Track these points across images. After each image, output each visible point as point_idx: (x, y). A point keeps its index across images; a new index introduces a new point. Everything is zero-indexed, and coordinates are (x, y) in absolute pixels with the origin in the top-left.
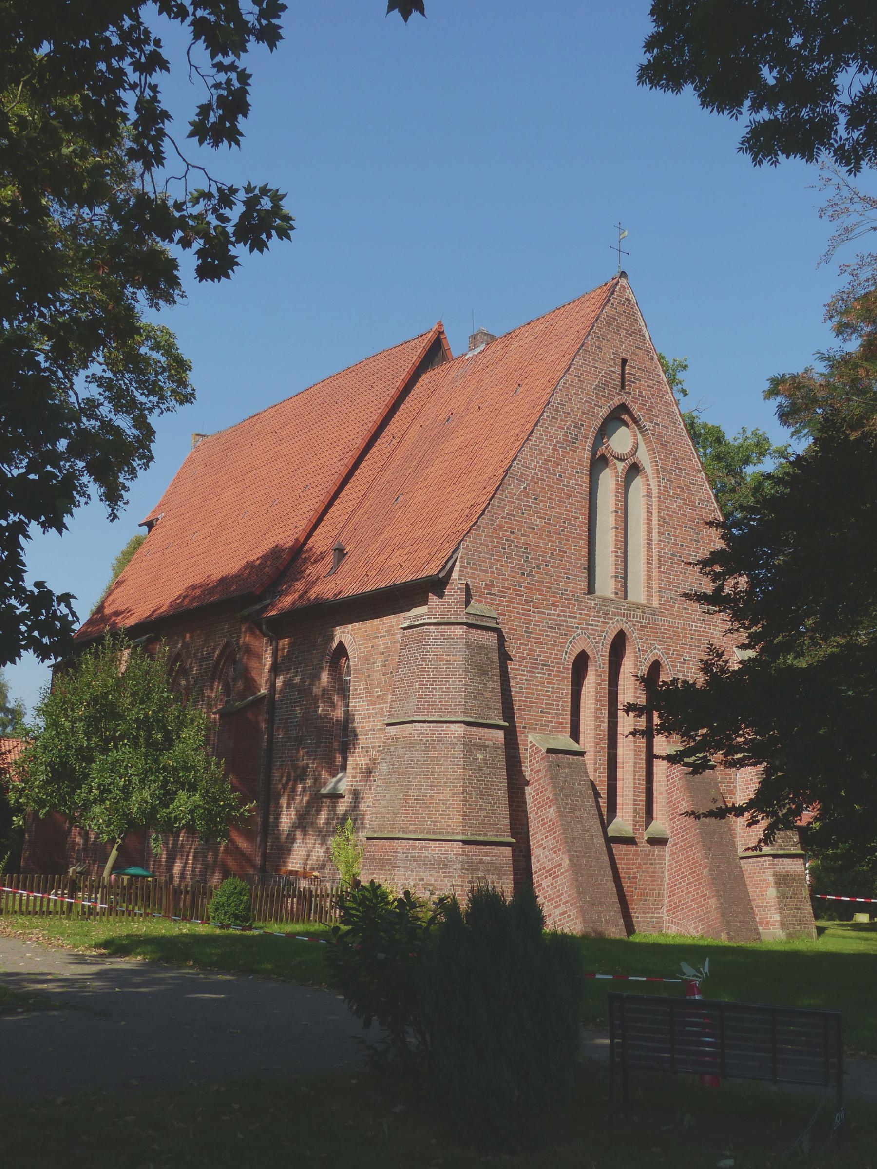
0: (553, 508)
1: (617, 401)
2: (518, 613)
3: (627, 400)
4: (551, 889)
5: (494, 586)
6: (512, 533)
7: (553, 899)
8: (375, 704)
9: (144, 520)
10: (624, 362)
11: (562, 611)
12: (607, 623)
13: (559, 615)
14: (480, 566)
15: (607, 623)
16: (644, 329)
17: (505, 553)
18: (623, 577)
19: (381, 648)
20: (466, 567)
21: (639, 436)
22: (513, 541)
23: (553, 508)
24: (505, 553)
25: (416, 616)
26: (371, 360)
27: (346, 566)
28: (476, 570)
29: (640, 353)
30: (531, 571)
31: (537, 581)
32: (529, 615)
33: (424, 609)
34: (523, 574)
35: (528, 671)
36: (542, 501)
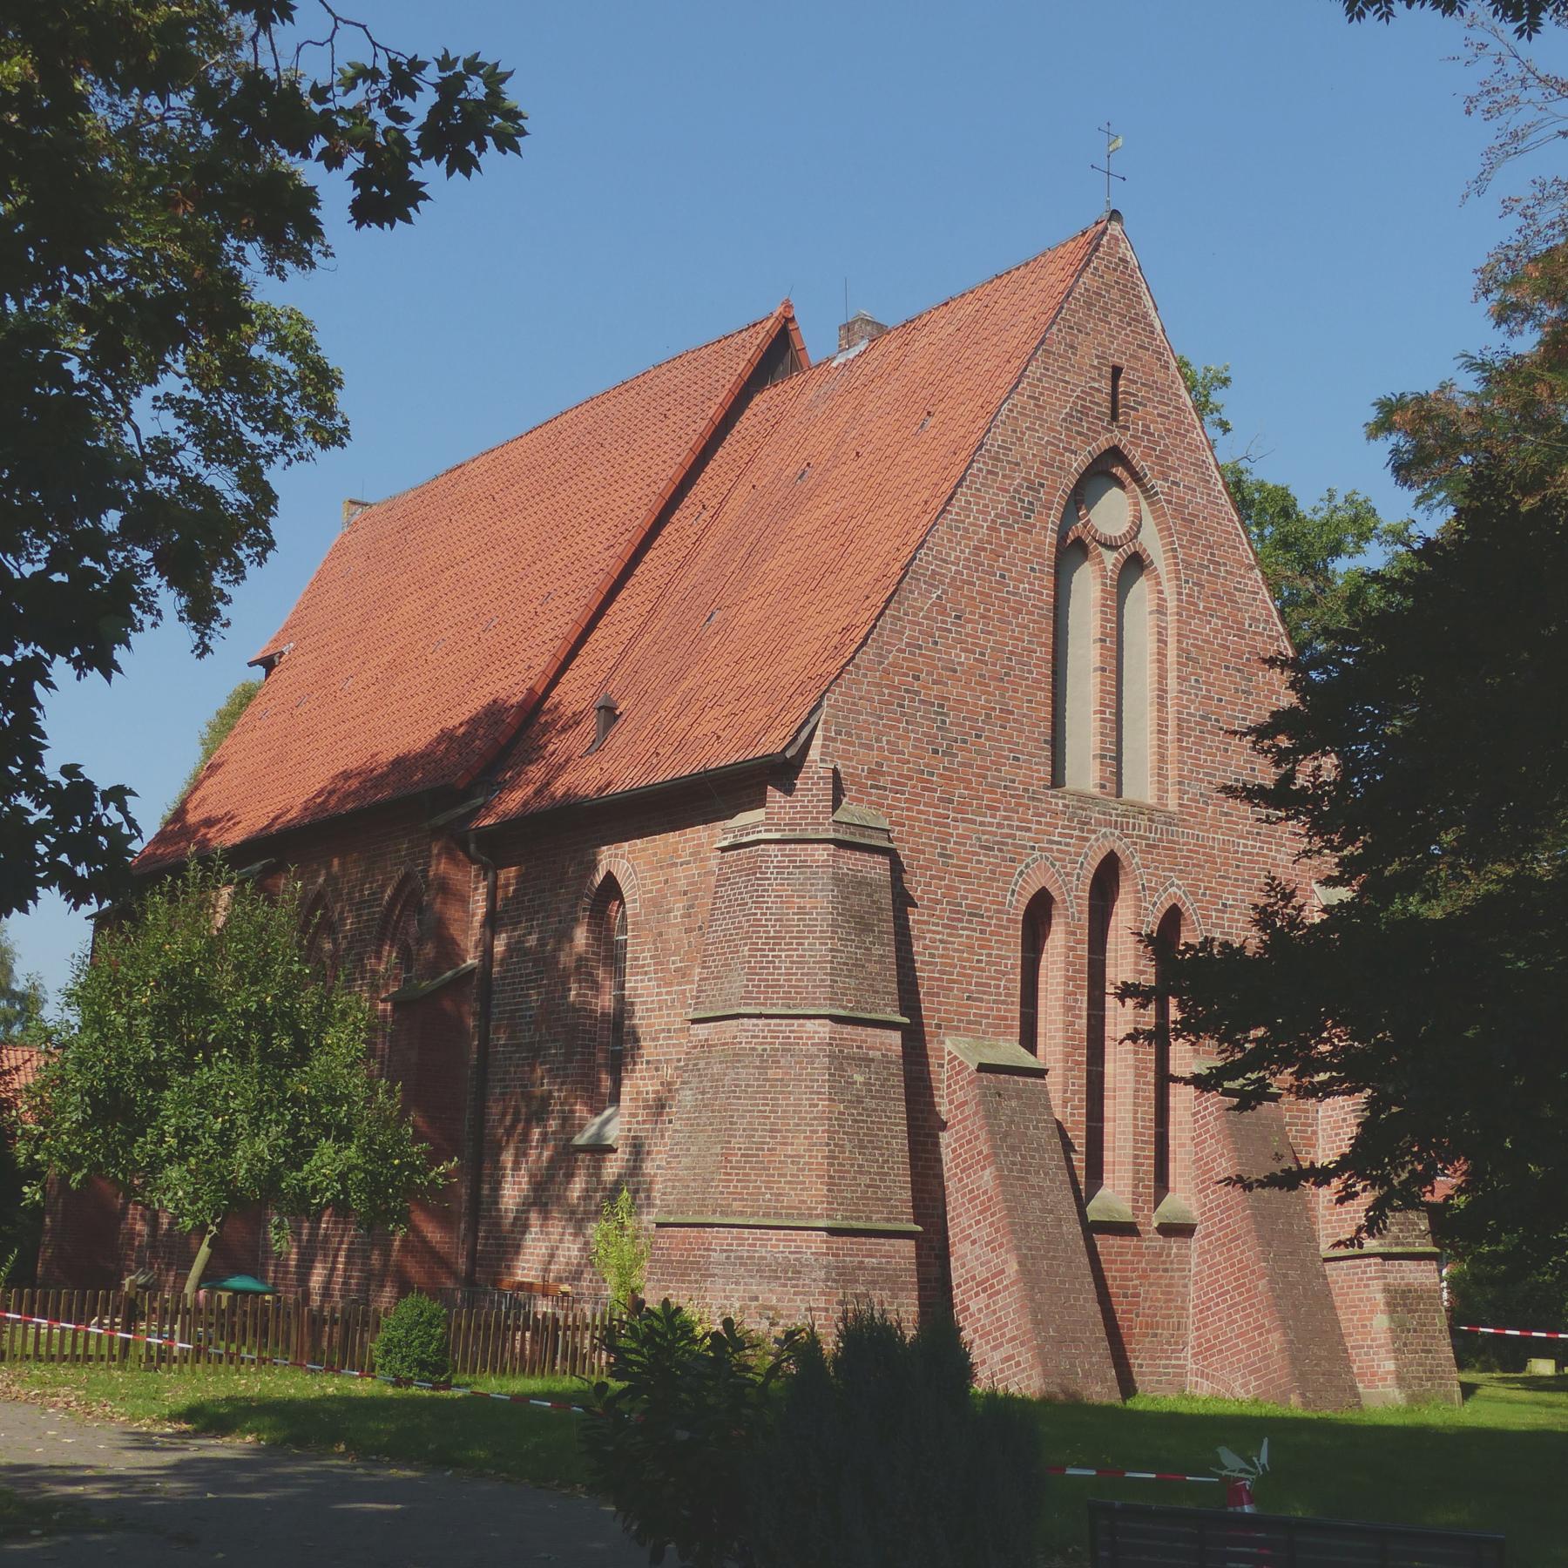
0: (990, 633)
1: (1103, 442)
3: (1122, 439)
6: (917, 678)
8: (671, 985)
10: (1117, 372)
11: (1006, 818)
13: (1000, 826)
14: (859, 737)
15: (1087, 839)
16: (1152, 313)
18: (1114, 758)
19: (682, 884)
20: (834, 740)
21: (1144, 505)
22: (917, 693)
23: (990, 633)
26: (664, 369)
27: (620, 737)
28: (851, 744)
30: (950, 747)
31: (961, 764)
32: (947, 826)
33: (757, 815)
34: (936, 752)
35: (945, 926)
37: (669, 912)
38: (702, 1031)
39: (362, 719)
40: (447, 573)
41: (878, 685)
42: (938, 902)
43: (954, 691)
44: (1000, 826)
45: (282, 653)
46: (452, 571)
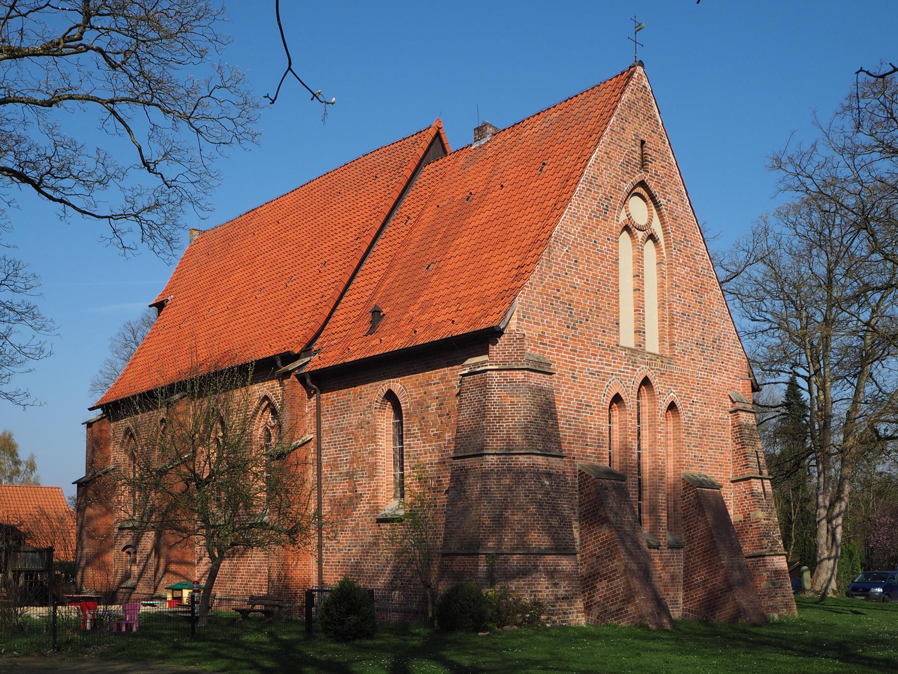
0: (590, 270)
1: (638, 178)
2: (566, 361)
3: (647, 178)
4: (607, 590)
5: (545, 337)
6: (558, 291)
7: (609, 598)
8: (431, 442)
9: (153, 302)
10: (643, 142)
11: (600, 360)
12: (635, 370)
13: (598, 363)
14: (534, 319)
15: (635, 370)
16: (657, 114)
17: (553, 308)
18: (640, 331)
19: (435, 393)
20: (522, 320)
21: (654, 211)
22: (559, 298)
23: (590, 270)
24: (553, 308)
25: (476, 364)
26: (369, 156)
27: (386, 326)
28: (530, 322)
29: (655, 136)
30: (574, 325)
31: (580, 333)
32: (574, 363)
33: (485, 358)
34: (568, 327)
35: (575, 411)
36: (581, 263)
37: (428, 407)
38: (458, 462)
39: (223, 327)
40: (258, 258)
41: (541, 294)
42: (572, 399)
43: (575, 297)
44: (598, 363)
45: (167, 300)
46: (261, 257)
